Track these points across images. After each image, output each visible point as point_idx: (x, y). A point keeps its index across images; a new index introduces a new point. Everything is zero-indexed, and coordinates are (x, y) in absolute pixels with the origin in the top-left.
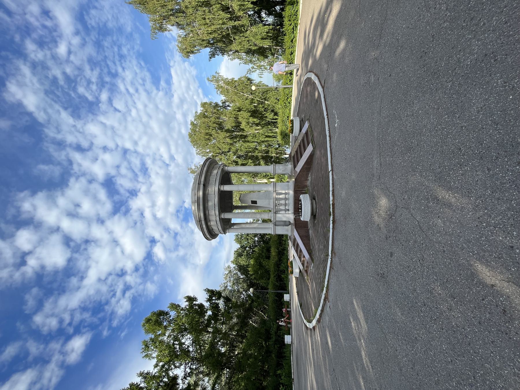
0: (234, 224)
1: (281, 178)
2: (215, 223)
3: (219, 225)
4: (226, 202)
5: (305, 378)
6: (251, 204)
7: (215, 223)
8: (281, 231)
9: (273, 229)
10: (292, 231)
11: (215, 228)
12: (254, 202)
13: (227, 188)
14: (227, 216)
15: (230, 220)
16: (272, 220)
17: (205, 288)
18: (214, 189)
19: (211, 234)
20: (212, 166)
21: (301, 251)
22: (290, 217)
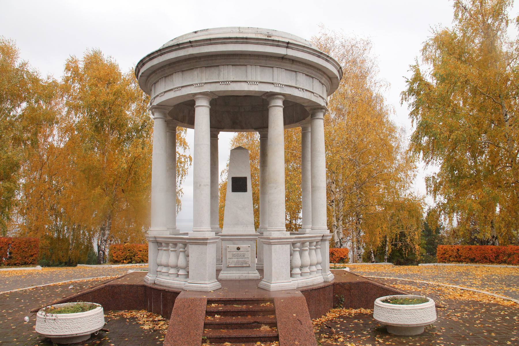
3: (178, 94)
11: (161, 87)
13: (277, 115)
14: (203, 114)
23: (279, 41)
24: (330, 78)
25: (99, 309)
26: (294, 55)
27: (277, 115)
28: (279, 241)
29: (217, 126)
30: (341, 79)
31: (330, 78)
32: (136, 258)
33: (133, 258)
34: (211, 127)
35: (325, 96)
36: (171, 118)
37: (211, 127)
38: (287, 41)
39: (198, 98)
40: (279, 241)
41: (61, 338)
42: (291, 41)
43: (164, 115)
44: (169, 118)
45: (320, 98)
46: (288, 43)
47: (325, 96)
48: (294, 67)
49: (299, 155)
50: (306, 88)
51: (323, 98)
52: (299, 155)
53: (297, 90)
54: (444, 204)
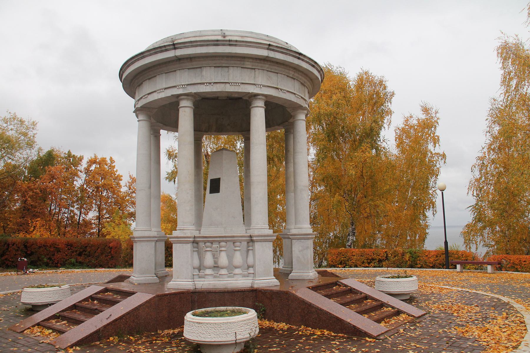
0: (157, 137)
1: (280, 245)
2: (159, 89)
3: (162, 95)
4: (222, 115)
5: (294, 155)
6: (211, 177)
7: (159, 89)
8: (145, 256)
9: (147, 234)
10: (145, 286)
11: (147, 88)
12: (215, 186)
13: (258, 116)
14: (186, 116)
15: (173, 125)
16: (175, 233)
17: (433, 104)
18: (259, 84)
19: (135, 76)
20: (308, 84)
21: (94, 312)
22: (181, 280)
23: (236, 41)
24: (311, 80)
25: (252, 313)
26: (199, 52)
27: (258, 116)
28: (263, 238)
29: (201, 129)
30: (322, 81)
31: (311, 80)
32: (350, 263)
33: (347, 262)
34: (195, 130)
35: (307, 98)
36: (155, 121)
37: (194, 131)
38: (268, 43)
39: (183, 99)
40: (263, 238)
41: (210, 345)
42: (271, 43)
43: (149, 117)
44: (153, 121)
45: (302, 100)
46: (269, 45)
47: (307, 98)
48: (195, 64)
49: (280, 154)
50: (288, 90)
51: (305, 100)
52: (280, 154)
53: (202, 86)
54: (74, 188)
